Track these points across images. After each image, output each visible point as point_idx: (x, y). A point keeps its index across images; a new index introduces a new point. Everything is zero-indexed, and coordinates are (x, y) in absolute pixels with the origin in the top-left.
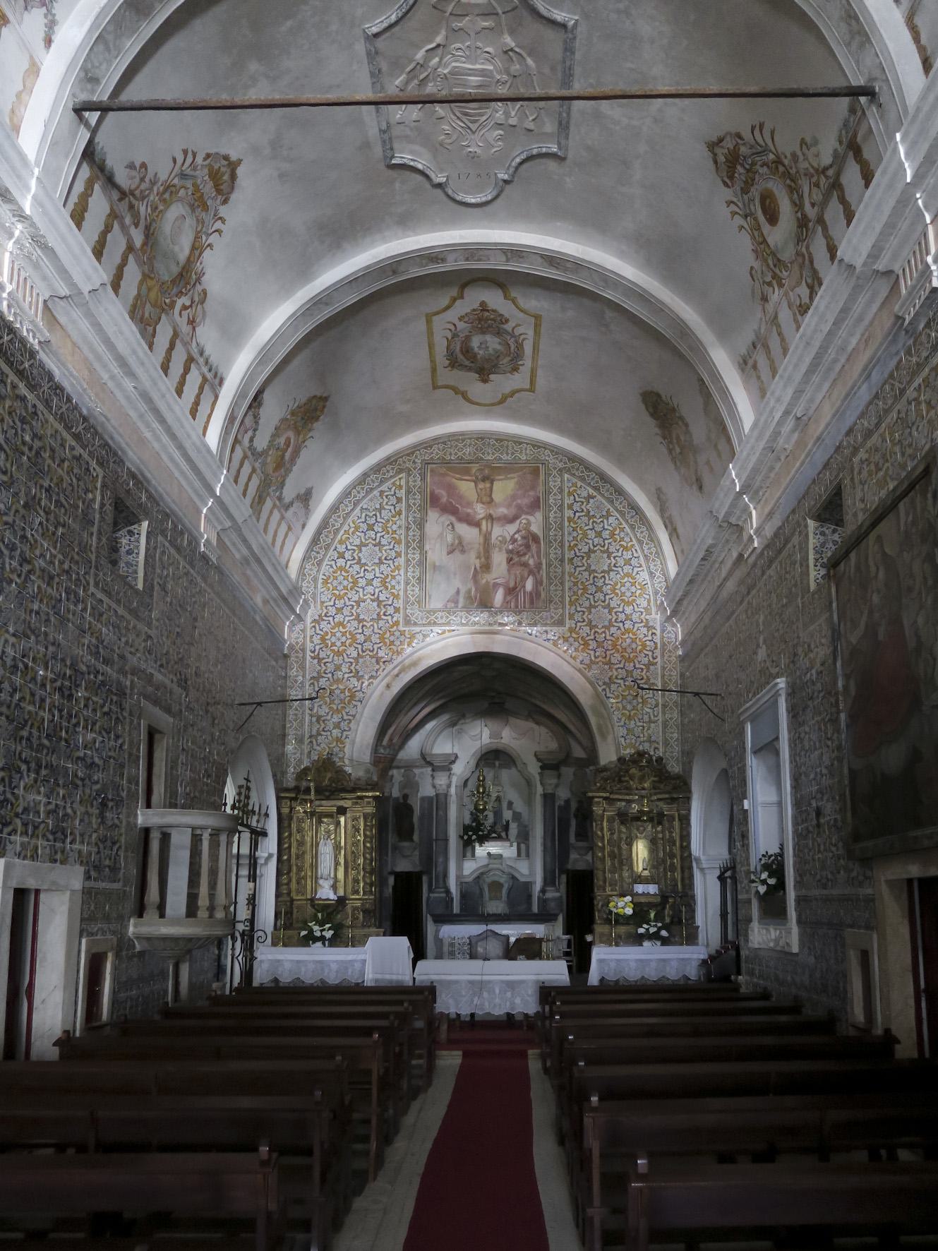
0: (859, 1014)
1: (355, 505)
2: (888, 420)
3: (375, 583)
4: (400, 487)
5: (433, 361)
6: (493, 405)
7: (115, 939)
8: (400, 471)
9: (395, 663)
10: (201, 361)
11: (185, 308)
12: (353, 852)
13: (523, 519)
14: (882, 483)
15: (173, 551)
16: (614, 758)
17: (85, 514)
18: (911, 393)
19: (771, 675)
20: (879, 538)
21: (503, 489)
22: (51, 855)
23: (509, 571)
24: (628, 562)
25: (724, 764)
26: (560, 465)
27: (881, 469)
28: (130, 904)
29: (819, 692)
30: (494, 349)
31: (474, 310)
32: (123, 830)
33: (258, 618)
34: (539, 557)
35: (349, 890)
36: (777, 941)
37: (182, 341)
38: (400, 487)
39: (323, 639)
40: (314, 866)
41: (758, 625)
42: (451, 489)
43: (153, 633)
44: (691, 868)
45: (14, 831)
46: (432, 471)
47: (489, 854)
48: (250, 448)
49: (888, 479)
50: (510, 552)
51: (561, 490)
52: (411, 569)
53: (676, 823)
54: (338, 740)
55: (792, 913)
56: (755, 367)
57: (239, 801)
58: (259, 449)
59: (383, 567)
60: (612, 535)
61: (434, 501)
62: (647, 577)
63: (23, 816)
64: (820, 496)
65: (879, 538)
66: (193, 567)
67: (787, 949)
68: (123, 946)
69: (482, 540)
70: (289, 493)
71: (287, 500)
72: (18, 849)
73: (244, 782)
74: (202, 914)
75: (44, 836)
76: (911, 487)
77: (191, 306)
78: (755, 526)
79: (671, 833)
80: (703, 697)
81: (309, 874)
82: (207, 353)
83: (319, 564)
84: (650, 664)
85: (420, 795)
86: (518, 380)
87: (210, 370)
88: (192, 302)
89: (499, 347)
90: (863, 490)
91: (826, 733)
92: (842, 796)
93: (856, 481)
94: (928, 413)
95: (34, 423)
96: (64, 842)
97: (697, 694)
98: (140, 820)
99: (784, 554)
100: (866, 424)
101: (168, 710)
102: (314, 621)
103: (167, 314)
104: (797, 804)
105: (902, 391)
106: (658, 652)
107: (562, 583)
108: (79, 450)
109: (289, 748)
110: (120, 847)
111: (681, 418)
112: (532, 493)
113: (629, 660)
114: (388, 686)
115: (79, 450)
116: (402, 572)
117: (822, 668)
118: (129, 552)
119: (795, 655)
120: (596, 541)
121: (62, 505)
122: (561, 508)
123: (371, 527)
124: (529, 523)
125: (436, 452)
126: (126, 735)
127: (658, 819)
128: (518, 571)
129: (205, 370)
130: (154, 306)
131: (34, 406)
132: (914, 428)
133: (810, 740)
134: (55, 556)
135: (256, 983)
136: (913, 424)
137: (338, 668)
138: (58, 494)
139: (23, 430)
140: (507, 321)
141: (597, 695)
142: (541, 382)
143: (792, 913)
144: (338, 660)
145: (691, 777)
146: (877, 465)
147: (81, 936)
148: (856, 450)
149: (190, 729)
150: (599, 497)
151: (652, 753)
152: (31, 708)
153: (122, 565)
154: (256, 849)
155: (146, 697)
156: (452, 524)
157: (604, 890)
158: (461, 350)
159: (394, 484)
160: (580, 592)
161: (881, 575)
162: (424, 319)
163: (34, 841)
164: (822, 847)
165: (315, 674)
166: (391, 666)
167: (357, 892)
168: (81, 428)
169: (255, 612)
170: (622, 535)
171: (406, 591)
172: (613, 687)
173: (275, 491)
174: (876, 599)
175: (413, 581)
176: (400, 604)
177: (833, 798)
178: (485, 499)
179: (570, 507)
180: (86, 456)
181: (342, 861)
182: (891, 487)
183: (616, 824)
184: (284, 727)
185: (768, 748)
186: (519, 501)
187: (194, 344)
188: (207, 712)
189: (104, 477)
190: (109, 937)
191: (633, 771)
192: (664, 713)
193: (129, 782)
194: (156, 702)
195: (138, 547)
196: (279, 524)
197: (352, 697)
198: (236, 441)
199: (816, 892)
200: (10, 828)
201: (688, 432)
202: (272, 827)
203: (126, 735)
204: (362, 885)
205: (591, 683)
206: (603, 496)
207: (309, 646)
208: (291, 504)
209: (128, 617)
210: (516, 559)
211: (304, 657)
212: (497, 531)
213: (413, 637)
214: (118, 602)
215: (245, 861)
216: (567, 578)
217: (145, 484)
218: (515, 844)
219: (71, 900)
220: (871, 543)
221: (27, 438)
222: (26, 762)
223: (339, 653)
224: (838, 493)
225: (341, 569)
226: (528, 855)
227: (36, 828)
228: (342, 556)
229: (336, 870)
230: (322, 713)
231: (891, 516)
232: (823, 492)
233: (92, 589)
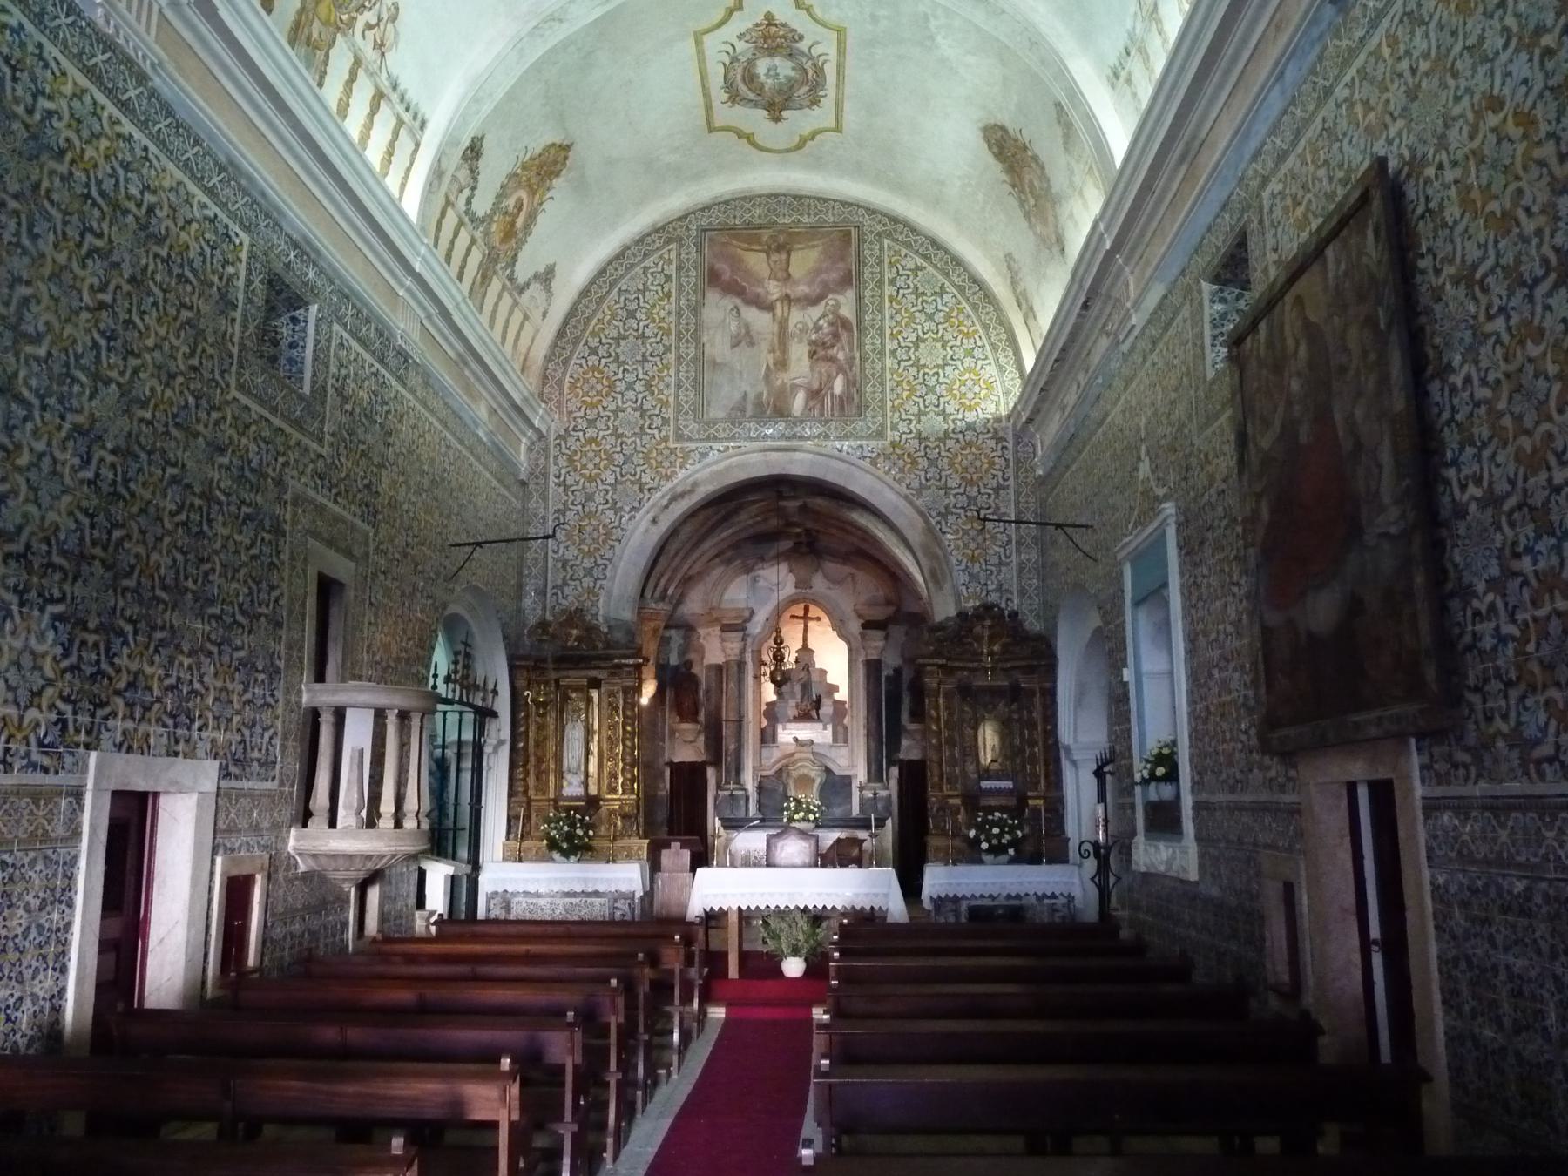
0: (1278, 969)
1: (612, 286)
2: (1309, 133)
3: (637, 386)
4: (670, 261)
5: (706, 94)
6: (788, 151)
7: (267, 856)
8: (669, 241)
9: (664, 489)
10: (395, 97)
11: (369, 27)
12: (609, 738)
13: (831, 300)
14: (1302, 224)
15: (354, 344)
16: (952, 612)
17: (223, 294)
18: (1341, 92)
19: (1156, 498)
20: (1299, 301)
21: (804, 261)
22: (168, 746)
23: (812, 369)
24: (970, 353)
25: (1095, 621)
26: (879, 228)
27: (1300, 204)
28: (290, 810)
29: (1221, 519)
30: (786, 77)
31: (757, 25)
32: (280, 711)
33: (481, 434)
34: (851, 350)
35: (605, 788)
36: (1169, 863)
37: (367, 70)
38: (670, 261)
39: (571, 460)
40: (559, 758)
41: (1138, 430)
42: (736, 262)
43: (325, 451)
44: (1058, 761)
45: (114, 714)
46: (711, 240)
47: (796, 739)
48: (466, 213)
49: (1310, 216)
50: (811, 343)
51: (880, 262)
52: (683, 368)
53: (1037, 699)
54: (590, 591)
55: (1188, 827)
56: (1129, 81)
57: (456, 672)
58: (480, 214)
59: (648, 366)
60: (948, 317)
61: (713, 278)
62: (995, 373)
63: (127, 694)
64: (1218, 248)
65: (1299, 301)
66: (385, 365)
67: (1182, 876)
68: (277, 864)
69: (776, 329)
70: (523, 272)
71: (521, 280)
72: (119, 738)
73: (461, 647)
74: (386, 822)
75: (158, 720)
76: (1344, 222)
77: (378, 25)
78: (1132, 296)
79: (1030, 712)
80: (1070, 530)
81: (552, 766)
82: (401, 87)
83: (566, 363)
84: (997, 490)
85: (706, 662)
86: (821, 116)
87: (407, 109)
88: (380, 19)
89: (792, 74)
90: (1275, 235)
91: (1231, 576)
92: (1254, 664)
93: (1267, 223)
94: (1365, 116)
95: (145, 171)
96: (189, 729)
97: (1058, 526)
98: (305, 699)
99: (1171, 332)
100: (1278, 142)
101: (349, 554)
102: (559, 437)
103: (344, 34)
104: (1194, 677)
105: (1328, 92)
106: (1010, 472)
107: (882, 384)
108: (213, 209)
109: (528, 602)
110: (276, 733)
111: (1035, 158)
112: (841, 265)
113: (971, 483)
114: (654, 521)
115: (213, 209)
116: (672, 372)
117: (1224, 486)
118: (293, 346)
119: (1188, 468)
120: (927, 326)
121: (188, 281)
122: (880, 283)
123: (632, 314)
124: (838, 305)
125: (717, 218)
126: (285, 585)
127: (1015, 694)
128: (824, 368)
129: (400, 109)
130: (326, 23)
131: (146, 149)
132: (1346, 141)
133: (1209, 585)
134: (178, 349)
135: (481, 913)
136: (1345, 135)
137: (590, 498)
138: (182, 266)
139: (127, 180)
140: (801, 38)
141: (929, 529)
142: (849, 119)
143: (1188, 827)
144: (591, 487)
145: (1055, 637)
146: (1294, 198)
147: (214, 852)
148: (1265, 181)
149: (382, 577)
150: (930, 269)
151: (1003, 605)
152: (141, 550)
153: (283, 361)
154: (482, 734)
155: (316, 535)
156: (736, 307)
157: (941, 789)
158: (743, 79)
159: (661, 257)
160: (905, 394)
161: (1303, 351)
162: (692, 40)
163: (142, 728)
164: (1228, 735)
165: (561, 506)
166: (659, 494)
167: (614, 791)
168: (216, 180)
169: (477, 425)
170: (961, 317)
171: (677, 397)
172: (951, 519)
173: (505, 268)
174: (1295, 385)
175: (687, 384)
176: (670, 413)
177: (1243, 667)
178: (779, 275)
179: (892, 282)
180: (222, 216)
181: (594, 748)
182: (1314, 226)
183: (957, 699)
184: (520, 574)
185: (1153, 595)
186: (824, 276)
187: (384, 75)
188: (405, 555)
189: (252, 245)
190: (257, 852)
191: (978, 629)
192: (1019, 552)
193: (290, 647)
194: (330, 543)
195: (303, 339)
196: (511, 313)
197: (608, 534)
198: (448, 203)
199: (1221, 797)
200: (107, 710)
201: (1044, 177)
202: (503, 705)
203: (285, 585)
204: (620, 780)
205: (921, 514)
206: (936, 267)
207: (553, 469)
208: (527, 285)
209: (288, 430)
210: (821, 353)
211: (546, 484)
212: (797, 317)
213: (686, 456)
214: (274, 410)
215: (469, 750)
216: (888, 376)
217: (313, 256)
218: (830, 727)
219: (199, 805)
220: (1287, 307)
221: (134, 191)
222: (130, 621)
223: (591, 479)
224: (1241, 242)
225: (594, 368)
226: (846, 741)
227: (147, 709)
228: (594, 352)
229: (587, 760)
230: (569, 556)
231: (1315, 268)
232: (1220, 242)
233: (234, 393)
